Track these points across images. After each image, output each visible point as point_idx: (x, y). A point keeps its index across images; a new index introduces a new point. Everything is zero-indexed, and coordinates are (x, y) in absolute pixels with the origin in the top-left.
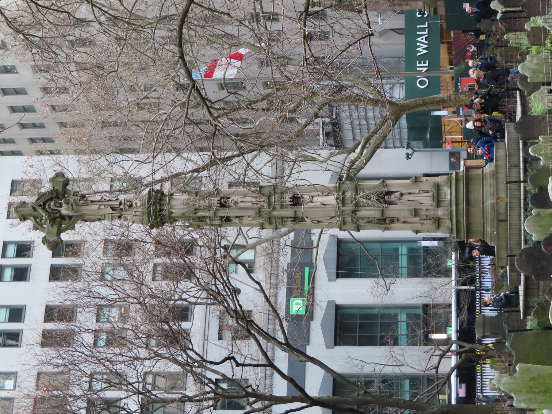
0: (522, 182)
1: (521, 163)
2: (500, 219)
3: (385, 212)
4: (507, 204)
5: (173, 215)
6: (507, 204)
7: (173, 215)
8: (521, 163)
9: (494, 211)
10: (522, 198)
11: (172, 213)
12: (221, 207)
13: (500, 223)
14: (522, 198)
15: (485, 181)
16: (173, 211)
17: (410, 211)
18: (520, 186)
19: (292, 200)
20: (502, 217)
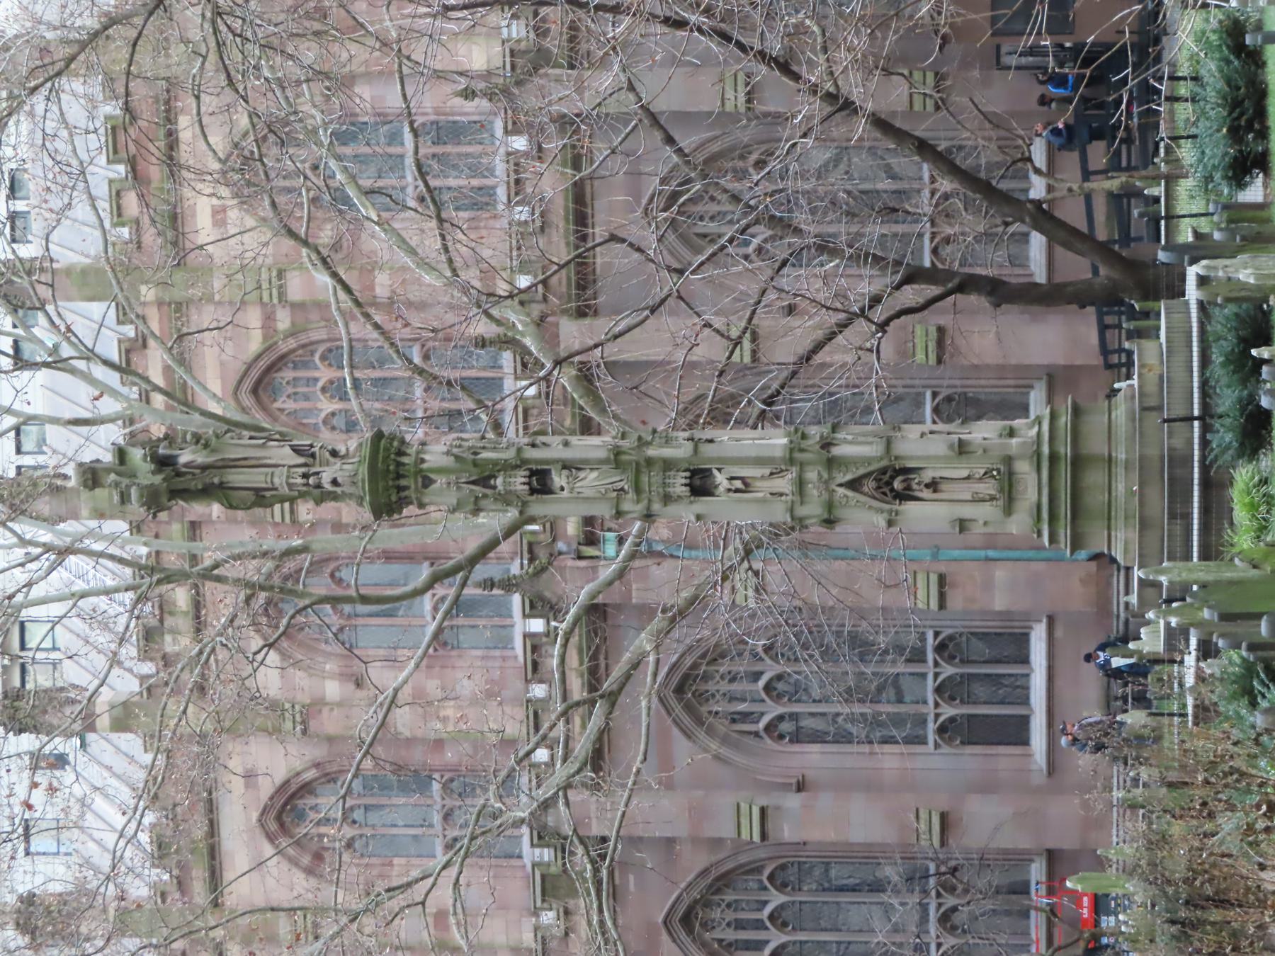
0: (1196, 418)
1: (1196, 447)
2: (1146, 405)
3: (893, 446)
4: (1161, 377)
5: (425, 466)
6: (1161, 377)
7: (425, 466)
8: (1196, 447)
9: (1134, 420)
10: (1195, 334)
11: (423, 461)
12: (532, 494)
13: (1147, 413)
14: (1195, 334)
15: (1113, 522)
16: (427, 457)
17: (951, 447)
18: (1192, 427)
19: (688, 481)
20: (1152, 402)
